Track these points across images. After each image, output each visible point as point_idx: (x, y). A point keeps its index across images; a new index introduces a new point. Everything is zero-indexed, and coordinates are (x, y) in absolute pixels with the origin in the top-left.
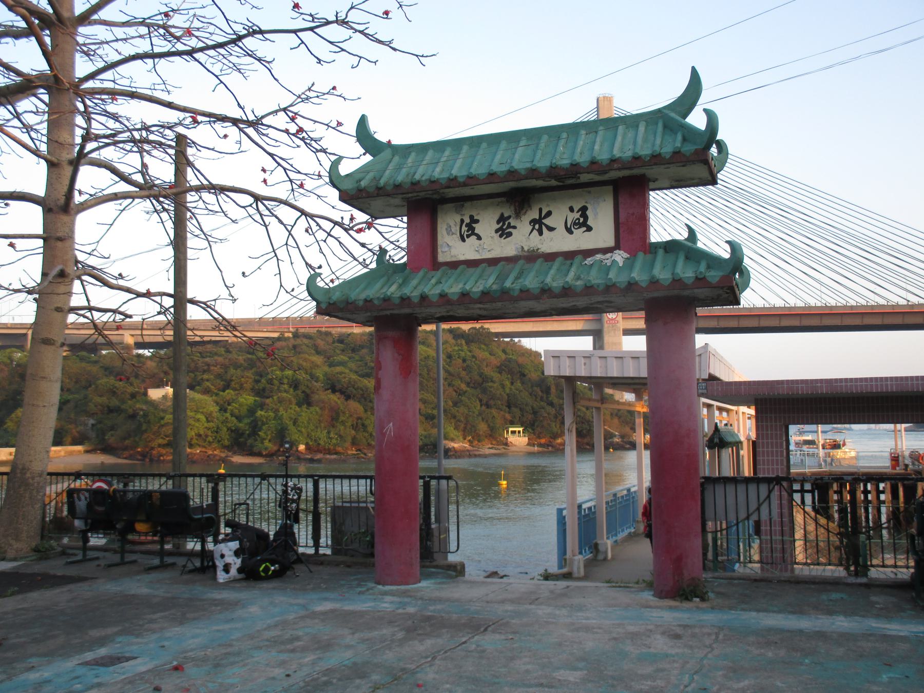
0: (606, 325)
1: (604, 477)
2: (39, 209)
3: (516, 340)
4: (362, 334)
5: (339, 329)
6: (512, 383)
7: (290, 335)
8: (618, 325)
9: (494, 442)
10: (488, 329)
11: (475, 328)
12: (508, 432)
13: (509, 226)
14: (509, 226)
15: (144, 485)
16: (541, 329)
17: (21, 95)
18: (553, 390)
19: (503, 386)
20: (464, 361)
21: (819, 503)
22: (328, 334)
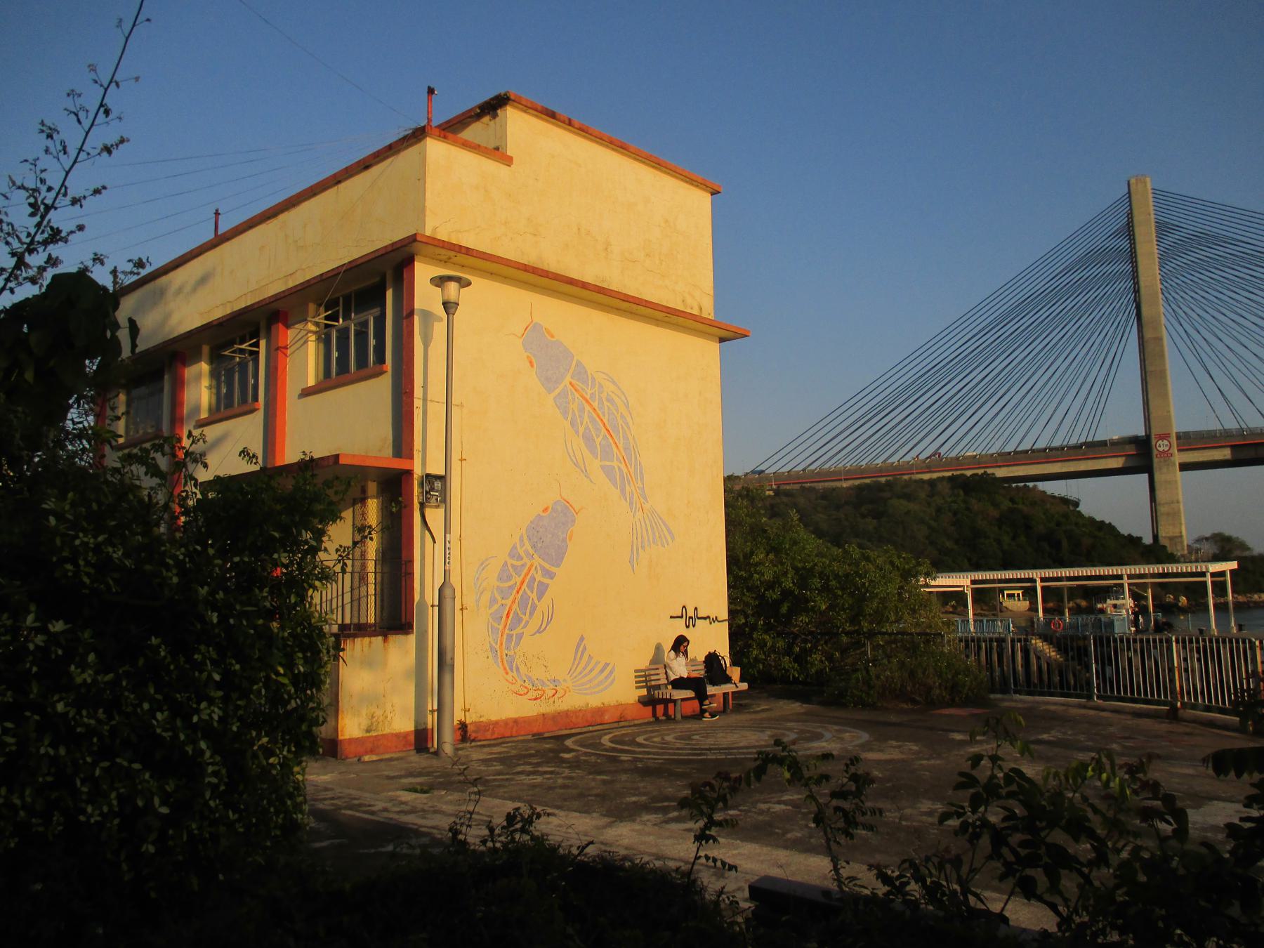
0: (1156, 460)
1: (1174, 644)
2: (707, 353)
3: (1031, 485)
4: (849, 488)
5: (826, 484)
6: (1014, 538)
7: (771, 493)
8: (1172, 459)
9: (985, 608)
10: (993, 474)
11: (977, 475)
12: (1003, 596)
13: (245, 456)
14: (245, 456)
15: (1080, 619)
16: (1072, 469)
17: (221, 320)
18: (1065, 544)
19: (999, 542)
20: (955, 514)
21: (733, 700)
22: (812, 490)
